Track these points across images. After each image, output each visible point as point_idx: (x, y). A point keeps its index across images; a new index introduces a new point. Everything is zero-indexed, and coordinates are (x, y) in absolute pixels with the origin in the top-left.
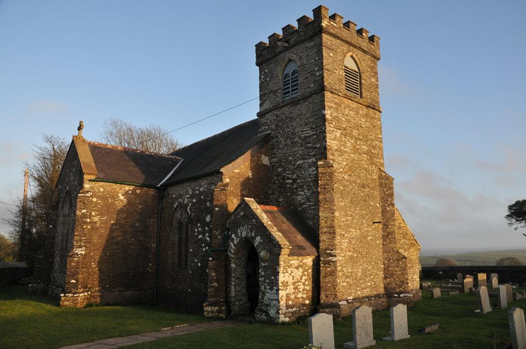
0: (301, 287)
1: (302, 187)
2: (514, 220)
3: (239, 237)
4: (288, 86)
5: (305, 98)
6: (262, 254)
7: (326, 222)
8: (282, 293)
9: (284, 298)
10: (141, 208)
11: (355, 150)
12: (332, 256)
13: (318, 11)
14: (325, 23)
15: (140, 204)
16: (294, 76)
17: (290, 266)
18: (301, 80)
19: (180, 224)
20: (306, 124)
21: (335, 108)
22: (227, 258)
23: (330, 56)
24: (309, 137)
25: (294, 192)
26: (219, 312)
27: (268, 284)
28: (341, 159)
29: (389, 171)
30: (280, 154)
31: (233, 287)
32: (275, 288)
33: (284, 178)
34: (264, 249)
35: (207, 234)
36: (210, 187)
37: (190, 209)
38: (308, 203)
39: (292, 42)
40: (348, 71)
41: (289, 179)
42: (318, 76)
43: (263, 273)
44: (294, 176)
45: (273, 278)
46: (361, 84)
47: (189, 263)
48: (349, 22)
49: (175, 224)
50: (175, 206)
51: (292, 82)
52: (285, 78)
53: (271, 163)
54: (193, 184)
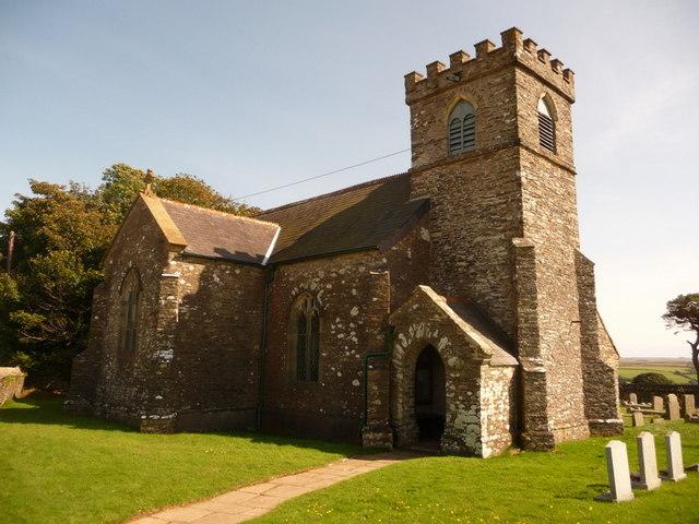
0: (502, 406)
1: (484, 272)
2: (673, 322)
3: (410, 337)
4: (457, 135)
5: (487, 154)
6: (452, 361)
7: (526, 321)
8: (483, 414)
9: (486, 421)
10: (241, 296)
12: (538, 365)
13: (509, 36)
14: (519, 52)
16: (466, 123)
17: (491, 378)
18: (479, 128)
19: (302, 319)
20: (490, 189)
21: (531, 171)
22: (392, 369)
25: (470, 278)
26: (385, 440)
27: (462, 402)
28: (537, 236)
30: (447, 226)
31: (400, 406)
32: (474, 407)
33: (453, 260)
34: (455, 355)
35: (353, 333)
36: (357, 269)
37: (322, 298)
38: (493, 294)
39: (467, 76)
40: (542, 118)
41: (462, 261)
42: (510, 125)
43: (453, 387)
44: (471, 258)
45: (469, 393)
46: (554, 136)
47: (321, 372)
48: (556, 61)
49: (294, 318)
50: (294, 293)
51: (465, 130)
52: (452, 124)
53: (432, 238)
54: (327, 263)
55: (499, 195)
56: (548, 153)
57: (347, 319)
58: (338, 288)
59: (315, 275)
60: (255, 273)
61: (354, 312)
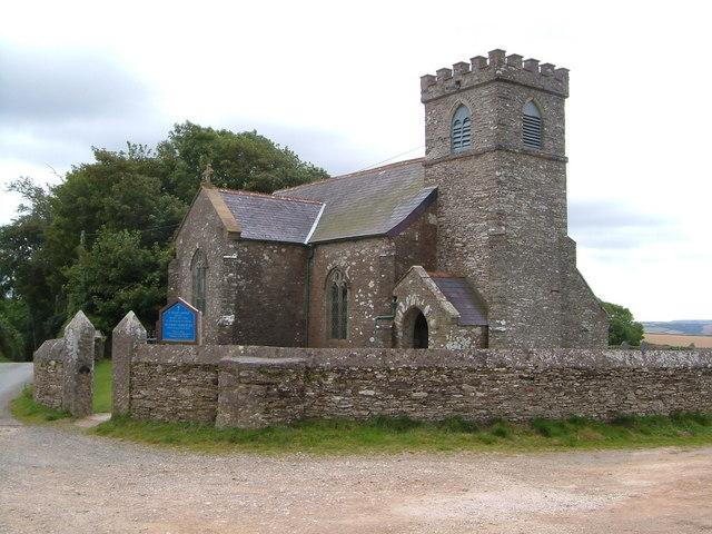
11: (534, 213)
15: (286, 265)
23: (507, 108)
24: (482, 199)
29: (572, 234)
40: (527, 120)
55: (484, 190)
56: (535, 149)
57: (366, 290)
58: (361, 266)
59: (344, 254)
60: (299, 251)
61: (371, 284)
